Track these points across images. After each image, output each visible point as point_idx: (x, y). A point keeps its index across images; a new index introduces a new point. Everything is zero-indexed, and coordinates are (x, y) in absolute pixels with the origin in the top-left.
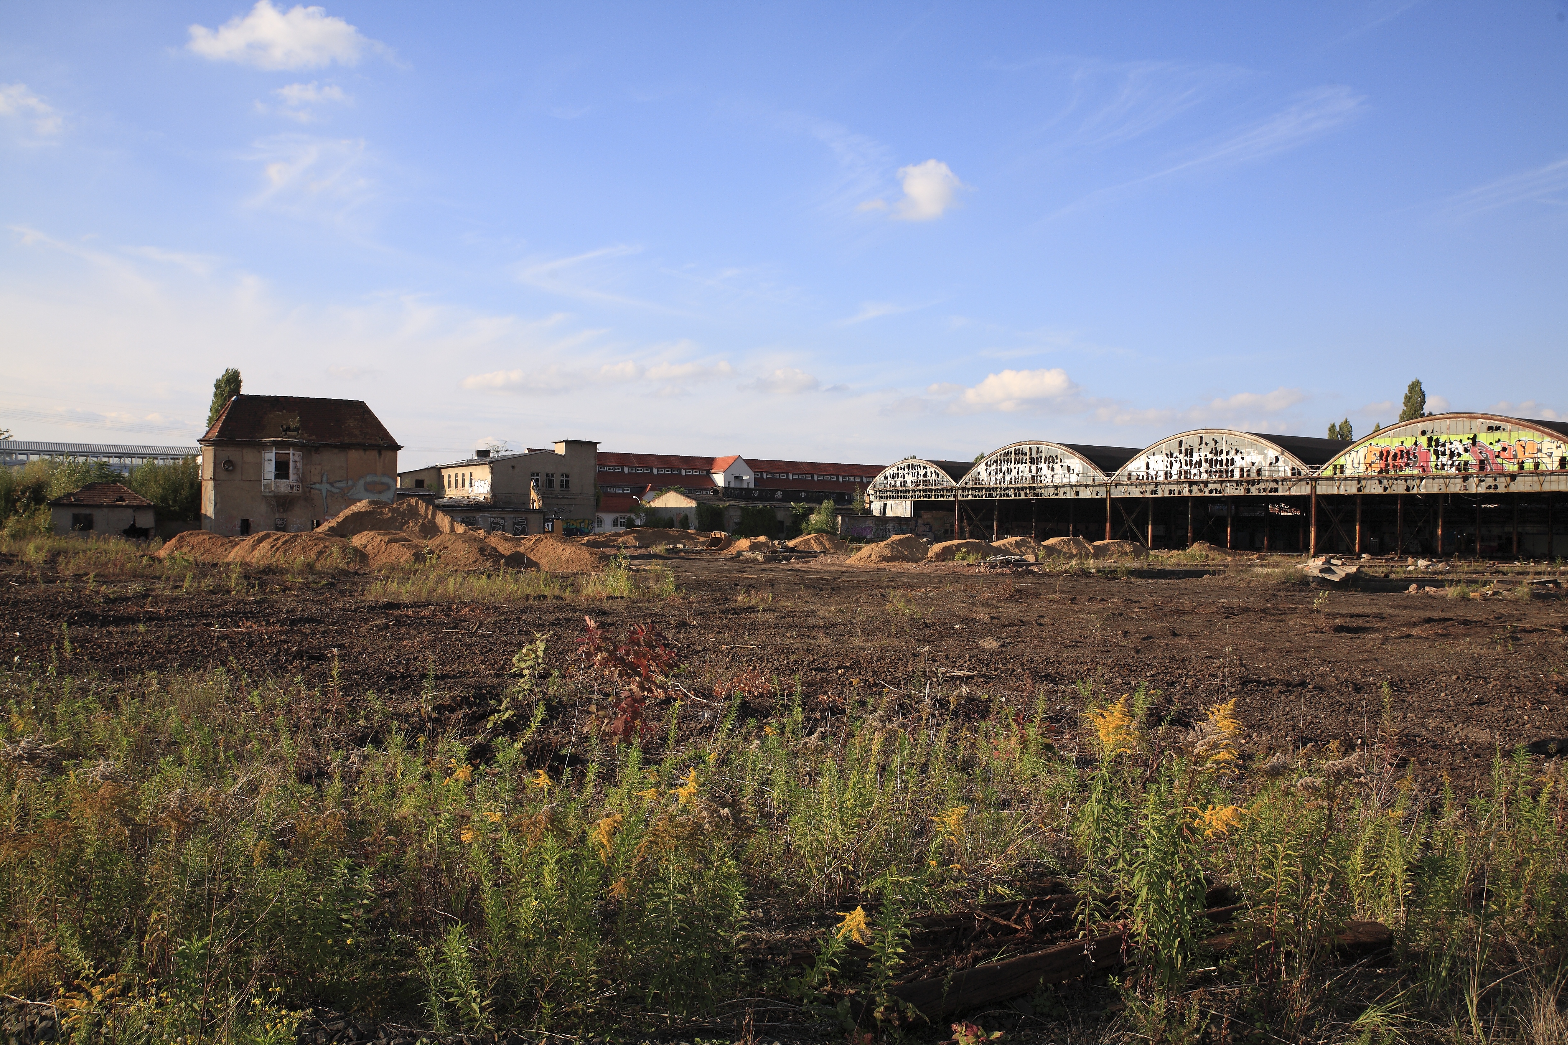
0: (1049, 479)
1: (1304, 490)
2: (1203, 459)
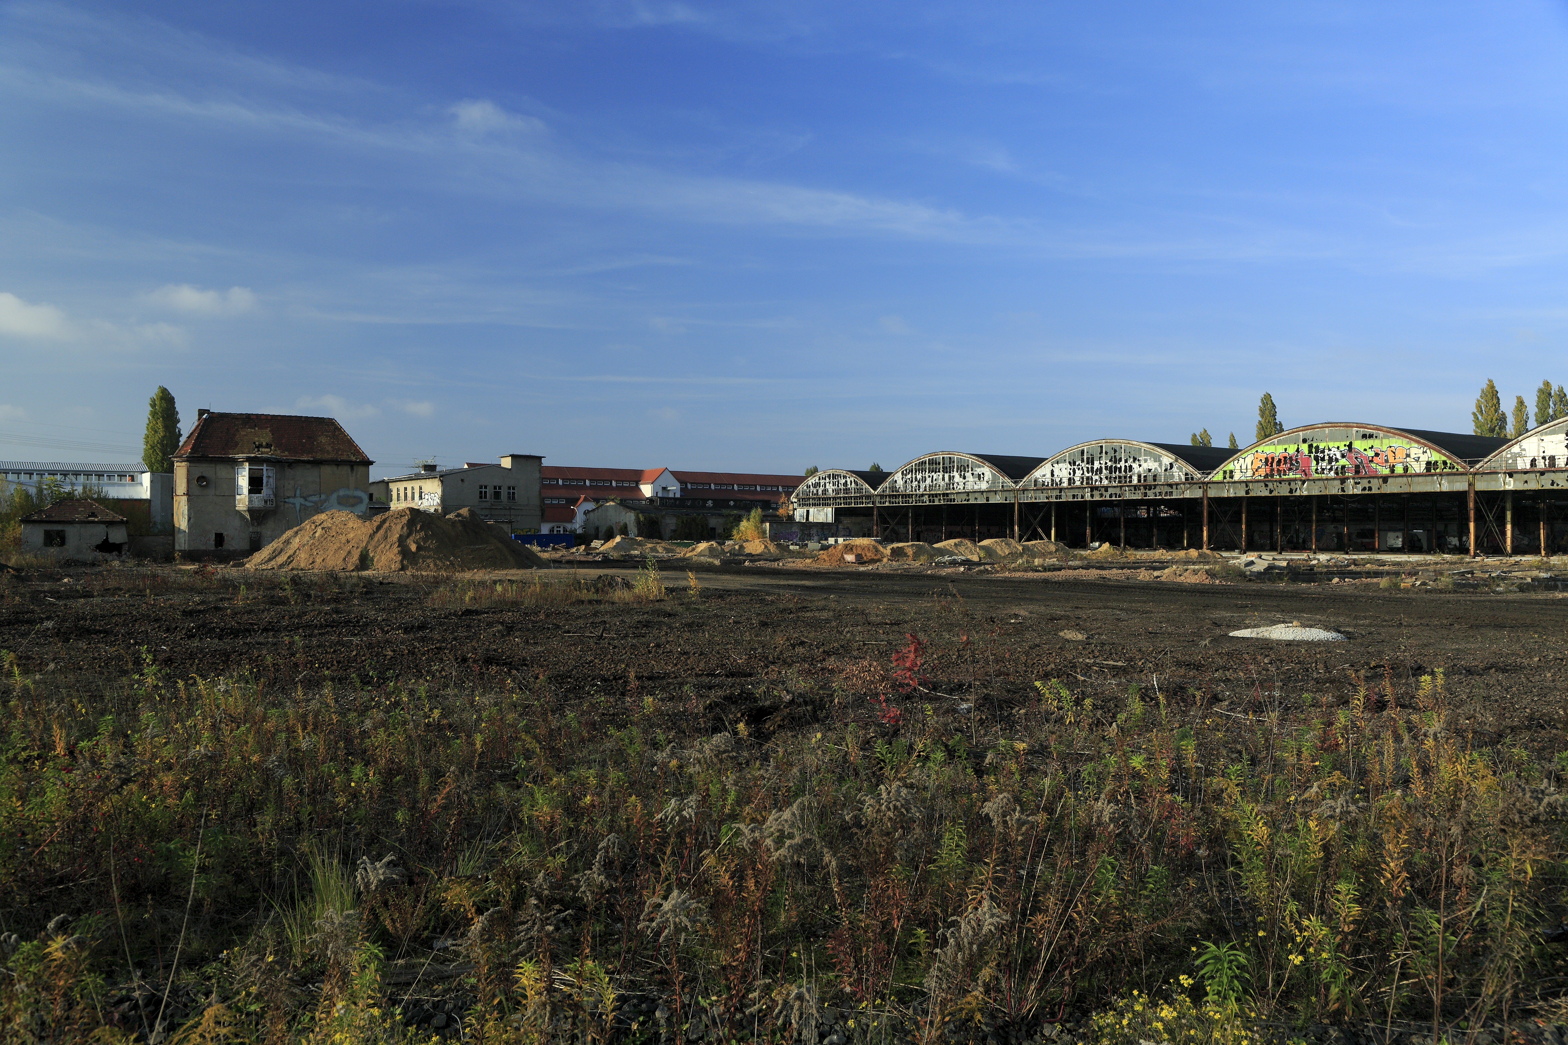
0: (961, 486)
1: (1197, 493)
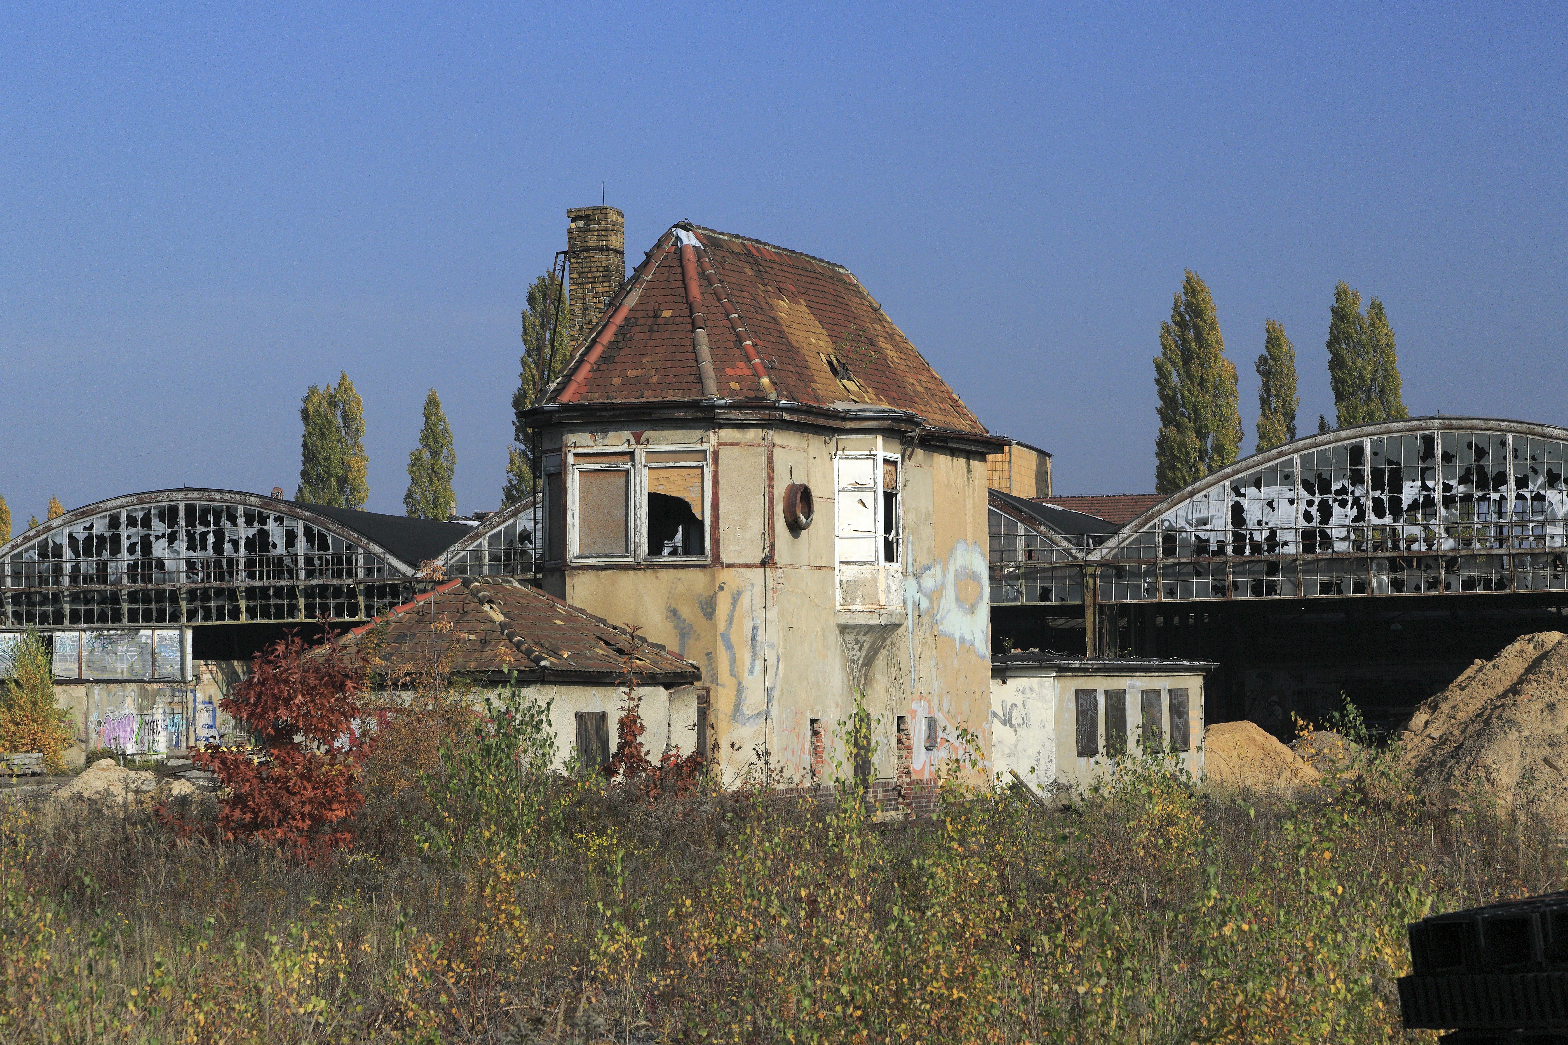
2: (1438, 496)
